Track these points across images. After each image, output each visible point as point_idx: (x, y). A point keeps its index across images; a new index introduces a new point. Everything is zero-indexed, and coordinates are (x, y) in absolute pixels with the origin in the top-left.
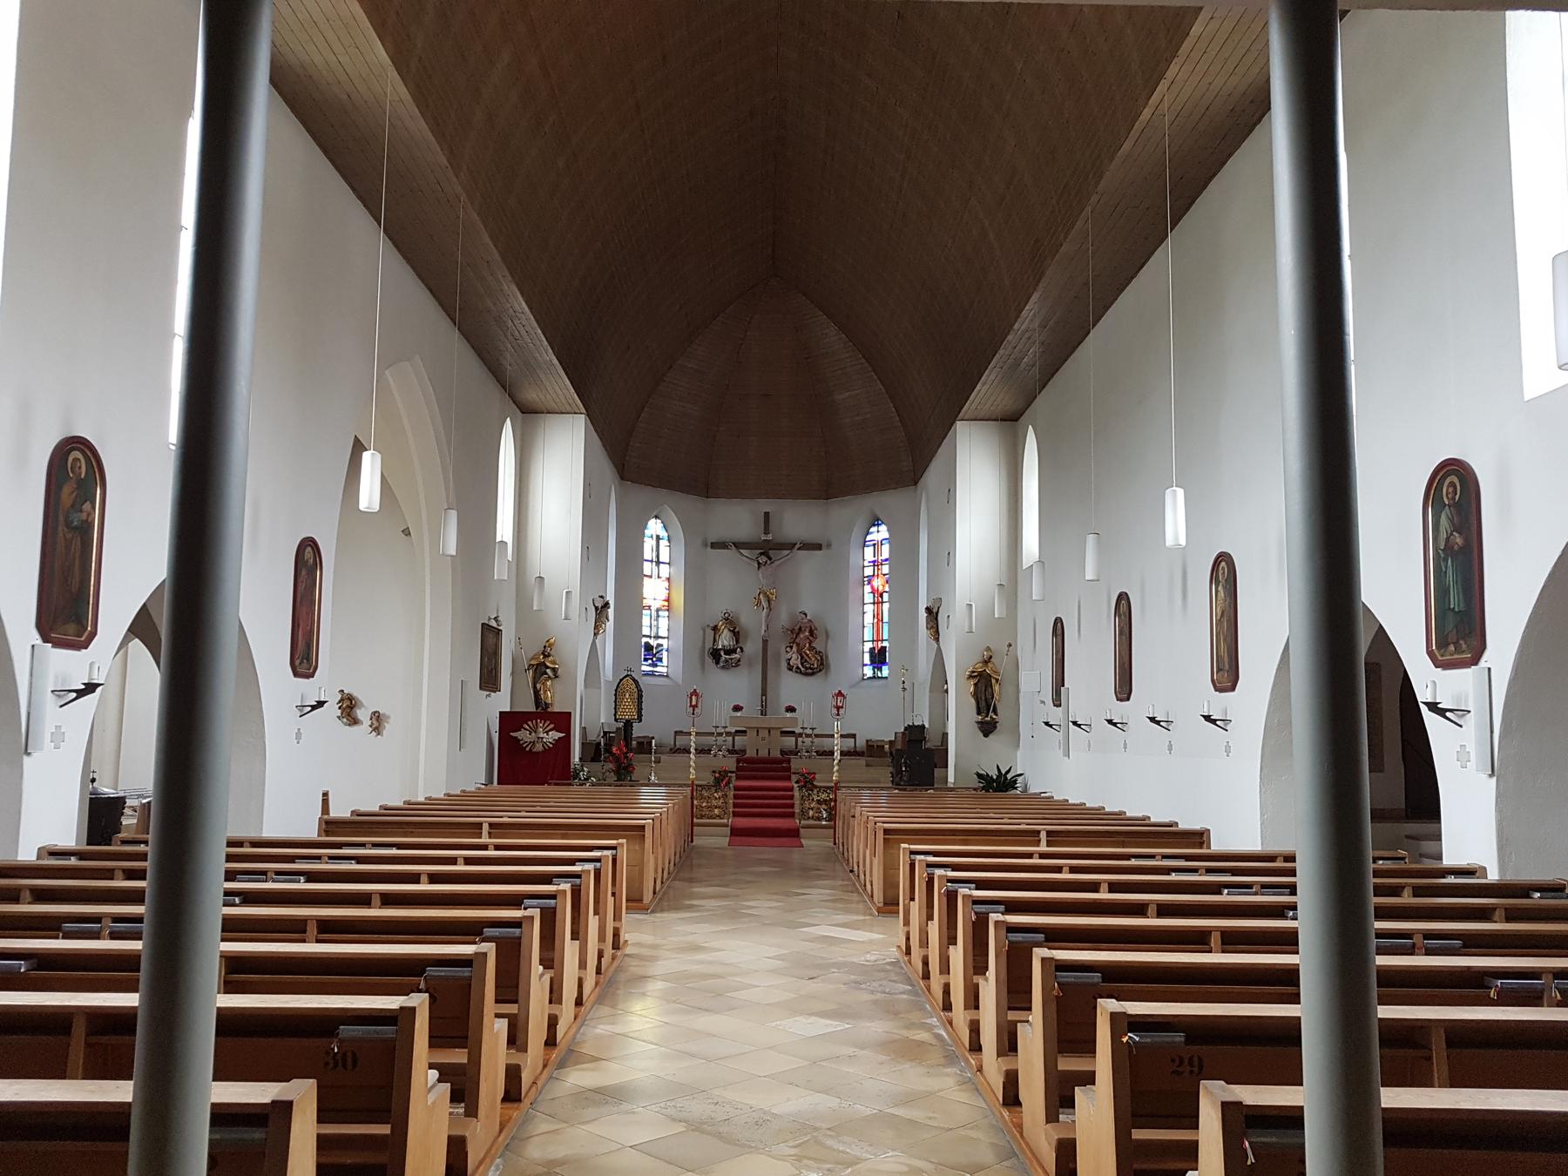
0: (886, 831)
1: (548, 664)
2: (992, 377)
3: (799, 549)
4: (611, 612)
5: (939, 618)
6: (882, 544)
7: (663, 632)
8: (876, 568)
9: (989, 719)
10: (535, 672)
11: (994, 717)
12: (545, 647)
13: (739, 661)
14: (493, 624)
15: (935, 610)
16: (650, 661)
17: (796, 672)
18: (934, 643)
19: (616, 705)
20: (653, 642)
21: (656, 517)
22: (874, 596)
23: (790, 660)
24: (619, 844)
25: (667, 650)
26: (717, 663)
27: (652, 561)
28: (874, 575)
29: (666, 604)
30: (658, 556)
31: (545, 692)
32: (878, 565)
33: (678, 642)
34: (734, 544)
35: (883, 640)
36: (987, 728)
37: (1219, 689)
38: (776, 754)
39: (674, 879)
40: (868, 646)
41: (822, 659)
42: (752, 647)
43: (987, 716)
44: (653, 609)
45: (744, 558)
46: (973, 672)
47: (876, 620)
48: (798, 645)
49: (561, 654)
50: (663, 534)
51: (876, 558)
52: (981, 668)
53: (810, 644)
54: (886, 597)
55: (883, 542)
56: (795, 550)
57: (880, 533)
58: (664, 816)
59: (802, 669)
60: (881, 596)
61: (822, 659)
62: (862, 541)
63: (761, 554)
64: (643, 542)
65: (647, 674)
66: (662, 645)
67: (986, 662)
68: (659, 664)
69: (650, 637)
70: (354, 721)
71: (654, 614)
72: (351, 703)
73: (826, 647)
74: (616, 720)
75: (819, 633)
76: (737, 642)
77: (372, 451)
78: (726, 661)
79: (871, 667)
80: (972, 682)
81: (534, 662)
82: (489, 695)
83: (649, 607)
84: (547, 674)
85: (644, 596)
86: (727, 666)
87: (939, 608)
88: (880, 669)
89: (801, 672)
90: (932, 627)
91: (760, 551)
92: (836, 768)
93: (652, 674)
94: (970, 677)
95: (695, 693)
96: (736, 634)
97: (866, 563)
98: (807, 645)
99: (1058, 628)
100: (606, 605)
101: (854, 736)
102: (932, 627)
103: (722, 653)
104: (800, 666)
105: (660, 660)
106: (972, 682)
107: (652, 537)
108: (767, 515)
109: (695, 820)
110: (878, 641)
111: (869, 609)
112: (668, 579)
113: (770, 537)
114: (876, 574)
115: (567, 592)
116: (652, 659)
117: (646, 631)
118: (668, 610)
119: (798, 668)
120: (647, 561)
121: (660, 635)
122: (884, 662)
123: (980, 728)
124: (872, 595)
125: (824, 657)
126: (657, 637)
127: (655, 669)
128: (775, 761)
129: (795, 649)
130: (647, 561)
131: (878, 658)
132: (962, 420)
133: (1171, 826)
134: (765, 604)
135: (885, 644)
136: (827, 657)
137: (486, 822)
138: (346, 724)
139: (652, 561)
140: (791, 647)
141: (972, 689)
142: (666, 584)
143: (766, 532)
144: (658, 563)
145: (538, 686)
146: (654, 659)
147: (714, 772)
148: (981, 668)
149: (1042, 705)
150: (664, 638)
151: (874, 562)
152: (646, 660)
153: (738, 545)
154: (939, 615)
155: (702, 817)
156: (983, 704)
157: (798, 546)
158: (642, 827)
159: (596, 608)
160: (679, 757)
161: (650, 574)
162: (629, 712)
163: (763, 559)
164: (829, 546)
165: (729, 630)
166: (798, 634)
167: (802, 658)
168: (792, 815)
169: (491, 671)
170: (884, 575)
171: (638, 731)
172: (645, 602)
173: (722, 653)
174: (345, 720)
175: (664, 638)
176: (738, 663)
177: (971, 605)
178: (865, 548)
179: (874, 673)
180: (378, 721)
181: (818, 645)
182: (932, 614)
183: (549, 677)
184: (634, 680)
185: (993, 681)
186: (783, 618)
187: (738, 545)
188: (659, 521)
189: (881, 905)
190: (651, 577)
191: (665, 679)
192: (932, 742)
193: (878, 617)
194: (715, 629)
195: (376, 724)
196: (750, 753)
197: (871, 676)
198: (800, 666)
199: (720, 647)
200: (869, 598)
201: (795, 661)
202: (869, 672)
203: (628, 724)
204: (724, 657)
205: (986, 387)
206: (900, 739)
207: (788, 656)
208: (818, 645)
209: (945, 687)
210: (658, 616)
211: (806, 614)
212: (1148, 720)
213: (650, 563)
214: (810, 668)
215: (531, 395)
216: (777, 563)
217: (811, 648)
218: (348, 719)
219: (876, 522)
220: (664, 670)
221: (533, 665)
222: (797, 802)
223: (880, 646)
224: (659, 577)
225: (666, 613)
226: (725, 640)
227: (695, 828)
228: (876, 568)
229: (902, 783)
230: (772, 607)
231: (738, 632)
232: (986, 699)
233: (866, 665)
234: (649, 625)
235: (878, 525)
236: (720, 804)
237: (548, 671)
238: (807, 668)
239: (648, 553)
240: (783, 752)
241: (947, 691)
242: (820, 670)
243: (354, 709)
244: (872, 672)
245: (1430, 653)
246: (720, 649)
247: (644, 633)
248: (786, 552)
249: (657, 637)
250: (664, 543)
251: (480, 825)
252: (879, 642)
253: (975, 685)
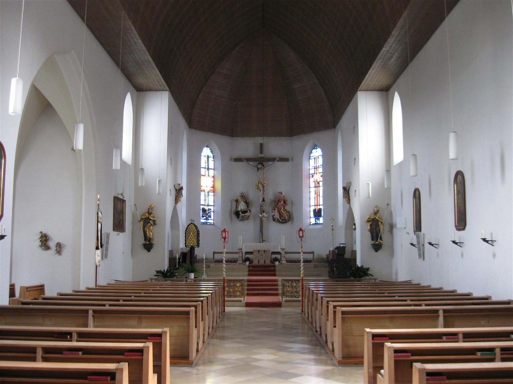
0: (343, 313)
1: (151, 218)
2: (377, 65)
3: (278, 161)
4: (184, 192)
5: (350, 192)
6: (318, 158)
7: (211, 203)
8: (316, 169)
9: (377, 243)
10: (144, 222)
11: (381, 241)
12: (149, 209)
13: (249, 216)
14: (121, 197)
15: (348, 188)
16: (205, 217)
17: (277, 222)
18: (348, 205)
19: (186, 239)
20: (206, 208)
21: (207, 147)
22: (315, 184)
23: (274, 215)
24: (163, 332)
25: (213, 212)
26: (238, 217)
27: (205, 168)
28: (315, 173)
29: (213, 189)
30: (208, 166)
31: (149, 232)
32: (317, 168)
33: (219, 208)
34: (245, 159)
35: (319, 205)
36: (377, 247)
37: (458, 229)
38: (268, 263)
39: (212, 338)
40: (312, 208)
41: (290, 215)
42: (254, 210)
43: (377, 241)
44: (206, 191)
45: (250, 166)
46: (370, 218)
47: (316, 195)
48: (278, 208)
49: (157, 214)
50: (211, 155)
51: (316, 165)
52: (374, 216)
53: (283, 208)
54: (321, 184)
55: (319, 157)
56: (276, 162)
57: (317, 152)
58: (210, 298)
59: (280, 220)
60: (319, 183)
61: (290, 215)
62: (308, 157)
63: (259, 163)
64: (201, 158)
65: (204, 224)
66: (210, 209)
67: (376, 214)
68: (209, 218)
69: (205, 205)
70: (48, 248)
71: (206, 194)
72: (46, 238)
73: (292, 209)
74: (186, 246)
75: (289, 202)
76: (248, 207)
77: (18, 78)
78: (243, 217)
79: (314, 219)
80: (163, 271)
81: (144, 217)
82: (118, 234)
83: (204, 190)
84: (150, 223)
85: (202, 185)
86: (243, 219)
87: (350, 187)
88: (319, 219)
89: (279, 222)
90: (346, 197)
91: (259, 162)
92: (302, 268)
93: (206, 223)
94: (368, 221)
95: (224, 231)
96: (247, 203)
97: (311, 168)
98: (282, 208)
99: (417, 194)
100: (181, 188)
101: (313, 253)
102: (346, 197)
103: (240, 213)
104: (279, 219)
105: (210, 217)
106: (163, 271)
107: (205, 156)
108: (261, 145)
109: (226, 299)
110: (317, 205)
111: (313, 190)
112: (213, 177)
113: (262, 156)
114: (316, 173)
115: (159, 181)
116: (206, 216)
117: (202, 202)
118: (213, 192)
119: (278, 220)
120: (202, 168)
121: (209, 204)
122: (320, 216)
123: (373, 248)
124: (314, 183)
125: (291, 214)
126: (208, 205)
127: (207, 221)
128: (268, 266)
129: (276, 210)
130: (202, 168)
131: (317, 214)
132: (360, 91)
133: (454, 292)
134: (261, 188)
135: (321, 207)
136: (292, 214)
137: (91, 309)
138: (44, 250)
139: (205, 168)
140: (275, 210)
141: (369, 227)
142: (213, 179)
143: (261, 152)
144: (208, 169)
145: (146, 229)
146: (207, 216)
147: (272, 212)
148: (374, 216)
149: (408, 235)
150: (212, 206)
151: (315, 167)
152: (203, 217)
153: (248, 160)
154: (350, 190)
155: (230, 296)
156: (375, 235)
157: (277, 159)
158: (188, 313)
159: (176, 190)
160: (218, 265)
161: (204, 175)
162: (194, 243)
163: (260, 166)
164: (292, 159)
165: (244, 202)
166: (278, 203)
167: (280, 215)
168: (277, 295)
169: (120, 222)
170: (320, 173)
171: (198, 252)
172: (202, 188)
173: (240, 213)
174: (43, 247)
175: (212, 206)
176: (248, 218)
177: (369, 183)
178: (310, 160)
179: (316, 221)
180: (59, 248)
181: (288, 208)
182: (346, 191)
183: (151, 225)
184: (195, 225)
185: (380, 223)
186: (270, 196)
187: (248, 160)
188: (208, 148)
189: (341, 359)
190: (204, 176)
191: (212, 226)
192: (348, 255)
193: (317, 194)
194: (237, 201)
195: (59, 249)
196: (255, 262)
197: (314, 223)
198: (279, 219)
199: (239, 210)
200: (312, 185)
201: (277, 216)
202: (313, 221)
203: (192, 249)
204: (241, 215)
205: (374, 71)
206: (331, 254)
207: (273, 214)
208: (288, 208)
209: (354, 227)
210: (209, 195)
211: (281, 193)
212: (452, 242)
213: (204, 169)
214: (284, 220)
215: (141, 80)
216: (267, 168)
217: (285, 210)
218: (45, 247)
219: (315, 147)
220: (212, 221)
221: (143, 219)
222: (280, 287)
223: (318, 208)
224: (209, 176)
225: (213, 194)
226: (242, 206)
227: (226, 303)
228: (316, 169)
229: (334, 277)
230: (265, 190)
231: (248, 202)
232: (376, 232)
233: (312, 218)
234: (204, 199)
235: (316, 148)
236: (240, 289)
237: (151, 221)
238: (282, 220)
239: (203, 164)
240: (271, 262)
241: (355, 229)
242: (289, 221)
243: (48, 242)
244: (315, 221)
245: (456, 226)
246: (240, 211)
247: (201, 204)
248: (271, 163)
249: (208, 205)
250: (211, 159)
251: (87, 311)
252: (318, 206)
253: (371, 225)
